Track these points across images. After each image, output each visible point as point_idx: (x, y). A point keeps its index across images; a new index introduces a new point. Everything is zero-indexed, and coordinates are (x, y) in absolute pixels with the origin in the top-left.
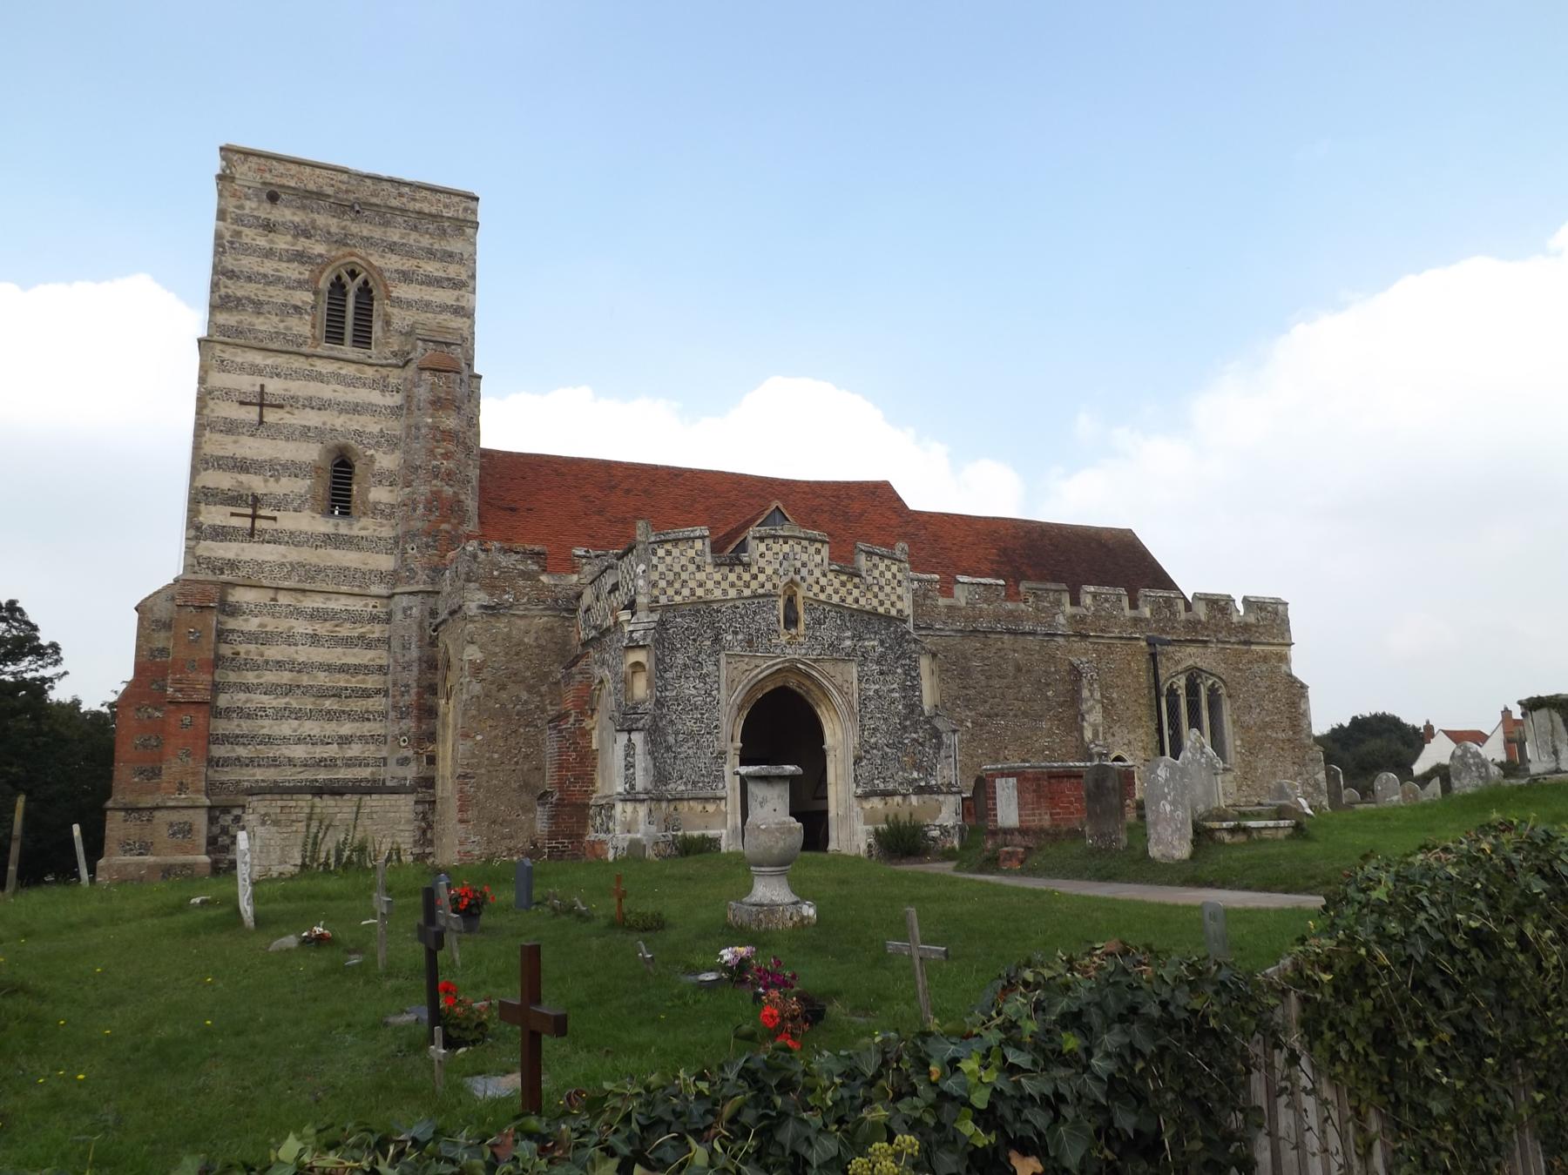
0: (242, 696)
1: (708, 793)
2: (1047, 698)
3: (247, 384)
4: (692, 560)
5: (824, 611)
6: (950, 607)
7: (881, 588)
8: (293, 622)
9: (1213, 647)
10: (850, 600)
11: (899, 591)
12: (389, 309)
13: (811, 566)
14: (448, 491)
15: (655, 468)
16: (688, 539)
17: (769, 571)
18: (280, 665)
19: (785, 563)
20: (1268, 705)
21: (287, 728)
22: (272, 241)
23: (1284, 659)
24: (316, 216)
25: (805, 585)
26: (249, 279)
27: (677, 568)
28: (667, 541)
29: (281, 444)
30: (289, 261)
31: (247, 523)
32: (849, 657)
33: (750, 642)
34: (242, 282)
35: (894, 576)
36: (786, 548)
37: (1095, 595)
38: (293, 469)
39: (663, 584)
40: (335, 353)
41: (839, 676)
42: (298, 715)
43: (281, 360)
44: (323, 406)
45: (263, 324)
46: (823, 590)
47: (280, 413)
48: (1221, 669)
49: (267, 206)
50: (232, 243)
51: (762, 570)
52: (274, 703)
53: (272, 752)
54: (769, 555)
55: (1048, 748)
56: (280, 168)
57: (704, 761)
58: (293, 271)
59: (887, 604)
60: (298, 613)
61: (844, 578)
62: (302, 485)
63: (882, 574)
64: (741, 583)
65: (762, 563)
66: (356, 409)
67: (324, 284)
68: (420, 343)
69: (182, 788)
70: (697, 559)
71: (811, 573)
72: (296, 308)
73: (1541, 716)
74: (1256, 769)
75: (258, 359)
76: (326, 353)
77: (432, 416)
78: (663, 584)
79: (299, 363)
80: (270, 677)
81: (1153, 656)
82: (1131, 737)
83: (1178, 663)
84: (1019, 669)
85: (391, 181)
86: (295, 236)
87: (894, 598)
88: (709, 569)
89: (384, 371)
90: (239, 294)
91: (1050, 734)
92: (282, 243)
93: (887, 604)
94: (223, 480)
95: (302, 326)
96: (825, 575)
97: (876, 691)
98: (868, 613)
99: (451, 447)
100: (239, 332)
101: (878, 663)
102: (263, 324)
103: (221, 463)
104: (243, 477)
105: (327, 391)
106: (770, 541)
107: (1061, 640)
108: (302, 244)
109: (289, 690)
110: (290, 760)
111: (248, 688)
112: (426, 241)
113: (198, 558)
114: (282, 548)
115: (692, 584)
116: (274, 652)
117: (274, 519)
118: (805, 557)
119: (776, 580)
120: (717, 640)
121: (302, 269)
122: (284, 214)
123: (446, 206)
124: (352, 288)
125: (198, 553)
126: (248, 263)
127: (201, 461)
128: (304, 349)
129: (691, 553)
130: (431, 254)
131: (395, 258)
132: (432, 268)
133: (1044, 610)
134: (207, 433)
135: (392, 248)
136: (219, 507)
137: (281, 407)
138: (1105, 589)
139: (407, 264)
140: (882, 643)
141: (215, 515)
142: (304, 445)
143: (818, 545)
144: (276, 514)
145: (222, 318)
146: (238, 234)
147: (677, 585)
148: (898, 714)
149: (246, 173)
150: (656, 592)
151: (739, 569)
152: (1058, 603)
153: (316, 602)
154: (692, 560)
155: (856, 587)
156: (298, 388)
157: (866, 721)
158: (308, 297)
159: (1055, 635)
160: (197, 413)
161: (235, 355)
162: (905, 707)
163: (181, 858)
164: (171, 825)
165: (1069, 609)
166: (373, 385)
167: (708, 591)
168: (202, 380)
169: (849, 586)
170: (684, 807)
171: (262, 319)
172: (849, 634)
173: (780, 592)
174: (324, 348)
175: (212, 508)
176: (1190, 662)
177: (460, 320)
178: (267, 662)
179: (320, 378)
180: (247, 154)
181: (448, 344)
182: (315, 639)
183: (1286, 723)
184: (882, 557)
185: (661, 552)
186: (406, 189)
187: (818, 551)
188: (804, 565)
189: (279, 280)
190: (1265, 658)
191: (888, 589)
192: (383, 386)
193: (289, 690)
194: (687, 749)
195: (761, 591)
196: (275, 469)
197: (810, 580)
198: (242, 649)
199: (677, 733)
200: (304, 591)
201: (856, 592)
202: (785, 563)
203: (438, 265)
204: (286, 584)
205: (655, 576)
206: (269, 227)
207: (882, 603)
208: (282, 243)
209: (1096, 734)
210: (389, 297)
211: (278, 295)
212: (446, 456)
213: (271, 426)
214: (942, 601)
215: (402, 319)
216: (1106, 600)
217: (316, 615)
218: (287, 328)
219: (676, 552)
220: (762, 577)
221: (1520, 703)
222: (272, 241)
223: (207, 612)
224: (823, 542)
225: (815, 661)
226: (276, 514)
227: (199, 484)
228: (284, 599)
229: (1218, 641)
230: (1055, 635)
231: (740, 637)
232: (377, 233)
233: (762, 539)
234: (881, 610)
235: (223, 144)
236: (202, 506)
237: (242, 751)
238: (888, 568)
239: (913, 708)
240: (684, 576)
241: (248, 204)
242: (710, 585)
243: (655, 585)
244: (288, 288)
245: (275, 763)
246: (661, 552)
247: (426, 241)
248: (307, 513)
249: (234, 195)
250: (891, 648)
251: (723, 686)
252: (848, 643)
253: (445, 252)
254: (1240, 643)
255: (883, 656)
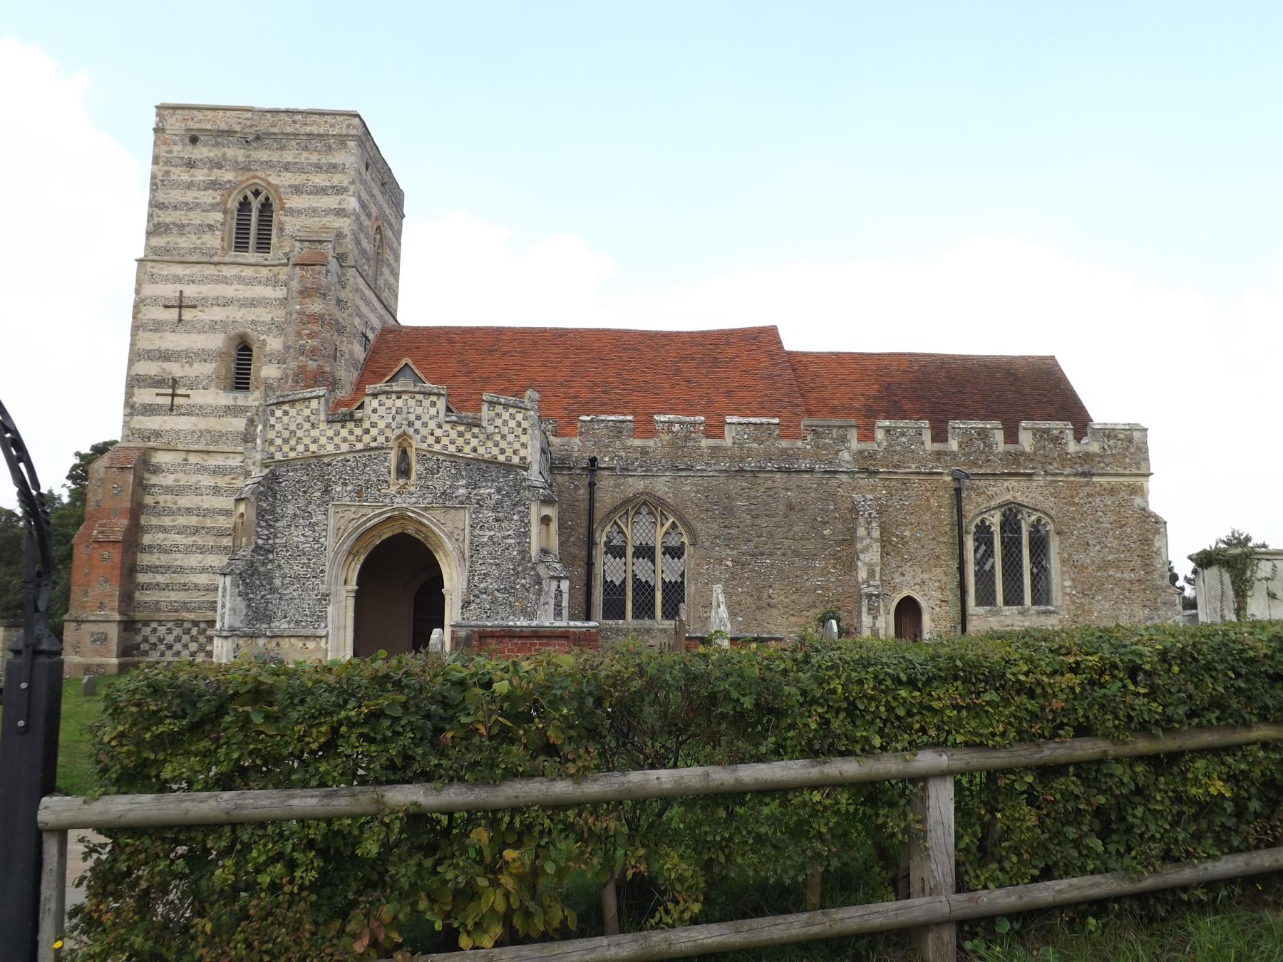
0: (161, 536)
1: (310, 631)
2: (823, 537)
3: (169, 291)
4: (308, 419)
5: (434, 463)
6: (713, 448)
7: (503, 437)
8: (200, 477)
9: (1040, 480)
10: (467, 449)
11: (524, 438)
12: (283, 219)
13: (425, 418)
14: (312, 365)
15: (598, 330)
16: (305, 399)
17: (381, 425)
18: (189, 511)
19: (398, 417)
20: (1111, 542)
21: (194, 560)
22: (192, 175)
23: (1140, 491)
24: (226, 150)
25: (418, 437)
26: (175, 208)
27: (293, 427)
28: (284, 403)
29: (195, 336)
30: (205, 189)
31: (168, 400)
32: (463, 503)
33: (359, 493)
34: (170, 211)
35: (519, 425)
36: (399, 403)
37: (888, 430)
38: (202, 356)
39: (279, 441)
40: (239, 260)
41: (449, 524)
42: (202, 550)
43: (195, 269)
44: (226, 303)
45: (184, 242)
46: (438, 441)
47: (195, 312)
48: (1050, 504)
49: (190, 147)
50: (162, 181)
51: (374, 425)
52: (185, 541)
53: (183, 579)
54: (381, 411)
55: (821, 587)
56: (199, 115)
57: (310, 600)
58: (208, 197)
59: (509, 452)
60: (203, 469)
61: (461, 428)
62: (209, 368)
63: (505, 423)
64: (353, 438)
65: (374, 418)
66: (253, 303)
67: (233, 204)
68: (298, 244)
69: (102, 606)
70: (312, 417)
71: (425, 425)
72: (210, 226)
73: (1212, 573)
74: (1091, 612)
75: (179, 270)
76: (232, 260)
77: (300, 304)
78: (279, 441)
79: (210, 271)
80: (182, 521)
81: (958, 491)
82: (926, 576)
83: (991, 498)
84: (791, 507)
85: (287, 112)
86: (210, 169)
87: (517, 446)
88: (323, 426)
89: (275, 270)
90: (167, 221)
91: (824, 572)
92: (201, 175)
93: (509, 452)
94: (149, 368)
95: (213, 241)
96: (440, 427)
97: (491, 538)
98: (485, 461)
99: (315, 328)
100: (167, 251)
101: (494, 510)
102: (184, 242)
103: (151, 355)
104: (166, 365)
105: (230, 291)
106: (383, 397)
107: (844, 478)
108: (216, 174)
109: (196, 531)
110: (196, 585)
111: (164, 530)
112: (314, 158)
113: (131, 429)
114: (194, 419)
115: (306, 441)
116: (184, 501)
117: (188, 396)
118: (419, 411)
119: (388, 433)
120: (326, 491)
121: (215, 194)
122: (203, 152)
123: (332, 126)
124: (256, 204)
125: (132, 426)
126: (176, 195)
127: (136, 355)
128: (215, 259)
129: (307, 412)
130: (318, 168)
131: (289, 175)
132: (319, 180)
133: (825, 447)
134: (140, 333)
135: (287, 167)
136: (148, 389)
137: (195, 307)
138: (901, 424)
139: (298, 179)
140: (499, 490)
141: (146, 396)
142: (212, 336)
143: (434, 398)
144: (189, 392)
145: (158, 241)
146: (168, 173)
147: (293, 442)
148: (512, 560)
149: (175, 125)
150: (272, 449)
151: (350, 425)
152: (843, 439)
153: (217, 461)
154: (308, 419)
155: (475, 436)
156: (208, 290)
157: (478, 567)
158: (219, 216)
159: (836, 472)
160: (134, 318)
161: (162, 269)
162: (520, 552)
163: (98, 660)
164: (92, 634)
165: (855, 445)
166: (268, 281)
167: (322, 447)
168: (137, 292)
169: (468, 436)
170: (285, 643)
171: (184, 239)
172: (463, 482)
173: (390, 445)
174: (232, 256)
175: (143, 391)
176: (1009, 497)
177: (341, 220)
178: (179, 509)
179: (225, 280)
180: (175, 108)
181: (320, 242)
182: (216, 490)
183: (1137, 562)
184: (506, 406)
185: (279, 413)
186: (299, 117)
187: (433, 404)
188: (418, 418)
189: (198, 205)
190: (1112, 491)
191: (510, 438)
192: (274, 282)
193: (196, 531)
194: (291, 591)
195: (373, 444)
196: (189, 356)
197: (424, 432)
198: (161, 499)
199: (284, 577)
200: (208, 452)
201: (474, 442)
202: (398, 417)
203: (324, 176)
204: (196, 447)
205: (272, 435)
206: (191, 164)
207: (502, 451)
208: (201, 175)
209: (871, 574)
210: (283, 208)
211: (196, 218)
212: (311, 336)
213: (188, 322)
214: (705, 443)
215: (289, 229)
216: (903, 434)
217: (218, 471)
218: (203, 244)
219: (292, 412)
220: (374, 432)
221: (1190, 558)
222: (192, 175)
223: (126, 472)
224: (439, 395)
225: (426, 509)
226: (189, 392)
227: (133, 373)
228: (193, 459)
229: (1047, 473)
230: (836, 472)
231: (349, 488)
232: (275, 157)
233: (375, 395)
234: (501, 458)
235: (158, 104)
236: (136, 390)
237: (161, 579)
238: (512, 417)
239: (524, 553)
240: (299, 433)
241: (175, 148)
242: (323, 440)
243: (271, 443)
244: (204, 211)
245: (185, 587)
246: (279, 413)
247: (314, 158)
248: (212, 390)
249: (165, 143)
250: (508, 495)
251: (330, 533)
252: (462, 491)
253: (330, 164)
254: (1076, 475)
255: (499, 504)
